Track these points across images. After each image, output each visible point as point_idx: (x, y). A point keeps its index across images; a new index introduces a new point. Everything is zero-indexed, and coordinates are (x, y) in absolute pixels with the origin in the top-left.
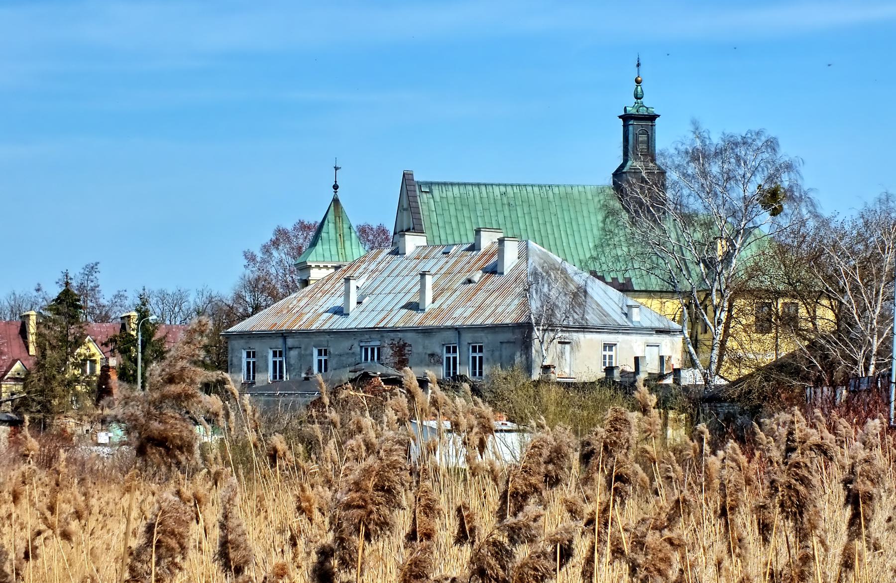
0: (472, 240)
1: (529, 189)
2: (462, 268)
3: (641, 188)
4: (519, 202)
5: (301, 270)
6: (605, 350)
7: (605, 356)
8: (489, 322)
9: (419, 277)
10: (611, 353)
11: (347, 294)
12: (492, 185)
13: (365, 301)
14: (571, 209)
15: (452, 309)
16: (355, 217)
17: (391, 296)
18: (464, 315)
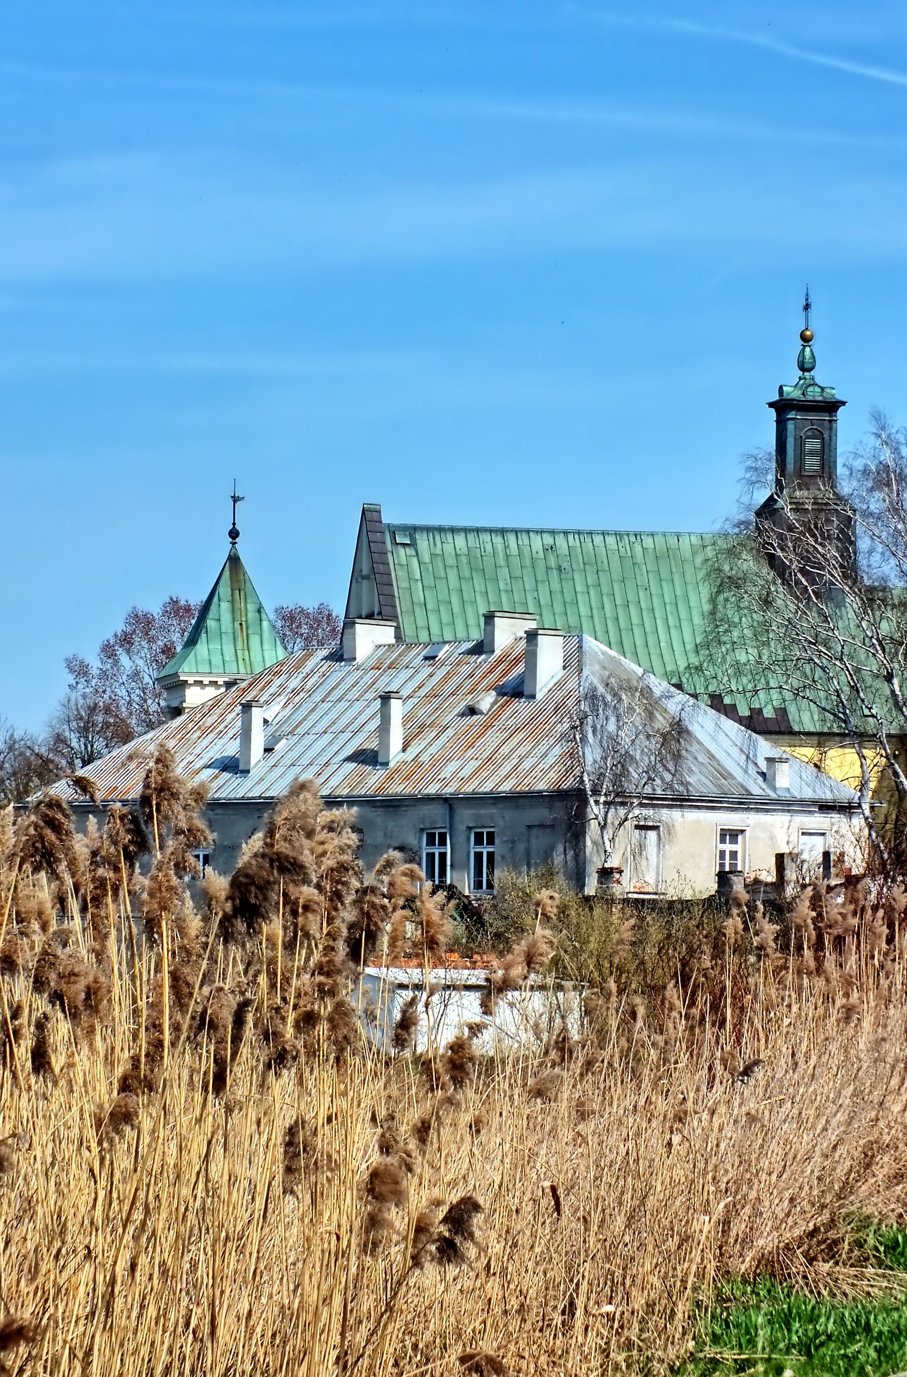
0: (476, 635)
1: (598, 539)
2: (459, 686)
3: (781, 537)
4: (578, 565)
5: (168, 688)
6: (723, 841)
7: (722, 853)
8: (506, 787)
9: (378, 704)
10: (733, 847)
11: (246, 734)
12: (528, 532)
13: (280, 747)
14: (677, 578)
15: (439, 762)
16: (276, 587)
17: (327, 738)
18: (462, 774)
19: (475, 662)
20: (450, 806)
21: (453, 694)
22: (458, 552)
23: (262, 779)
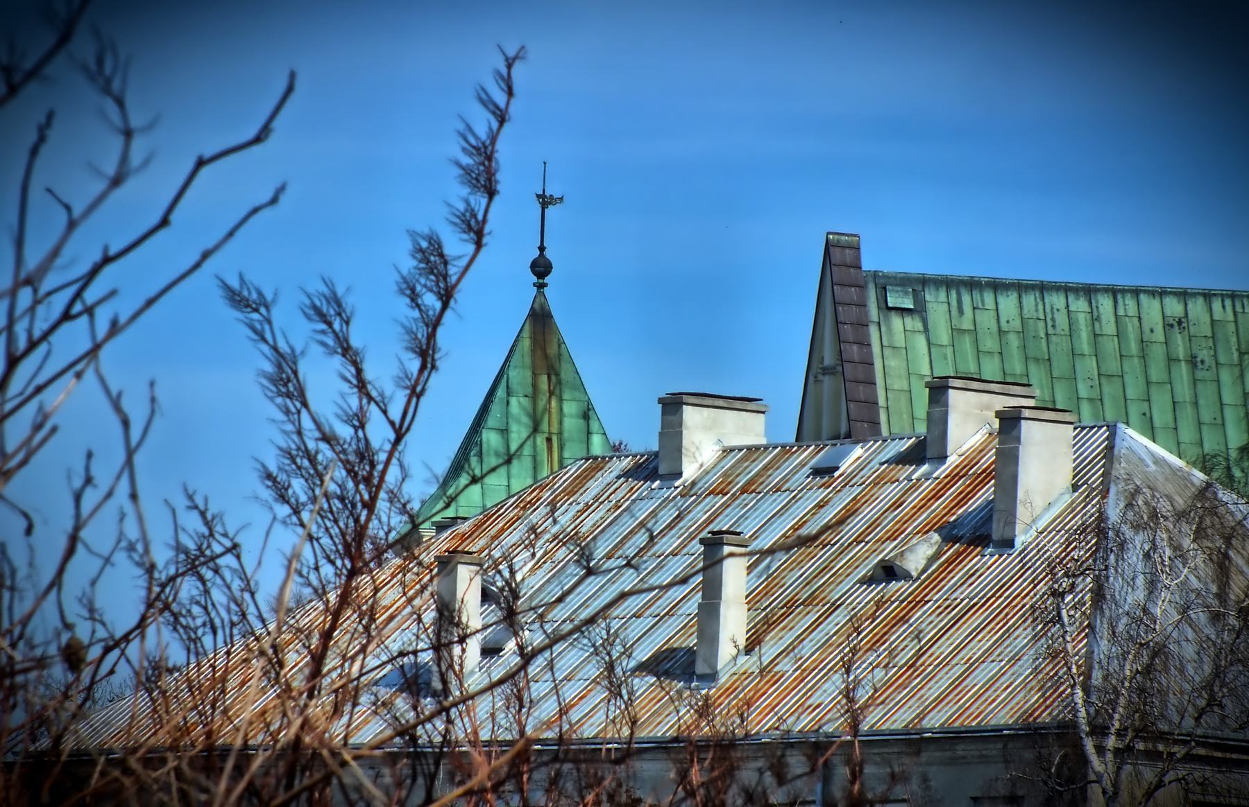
2: (873, 525)
8: (935, 721)
19: (909, 479)
21: (858, 541)
22: (1004, 326)
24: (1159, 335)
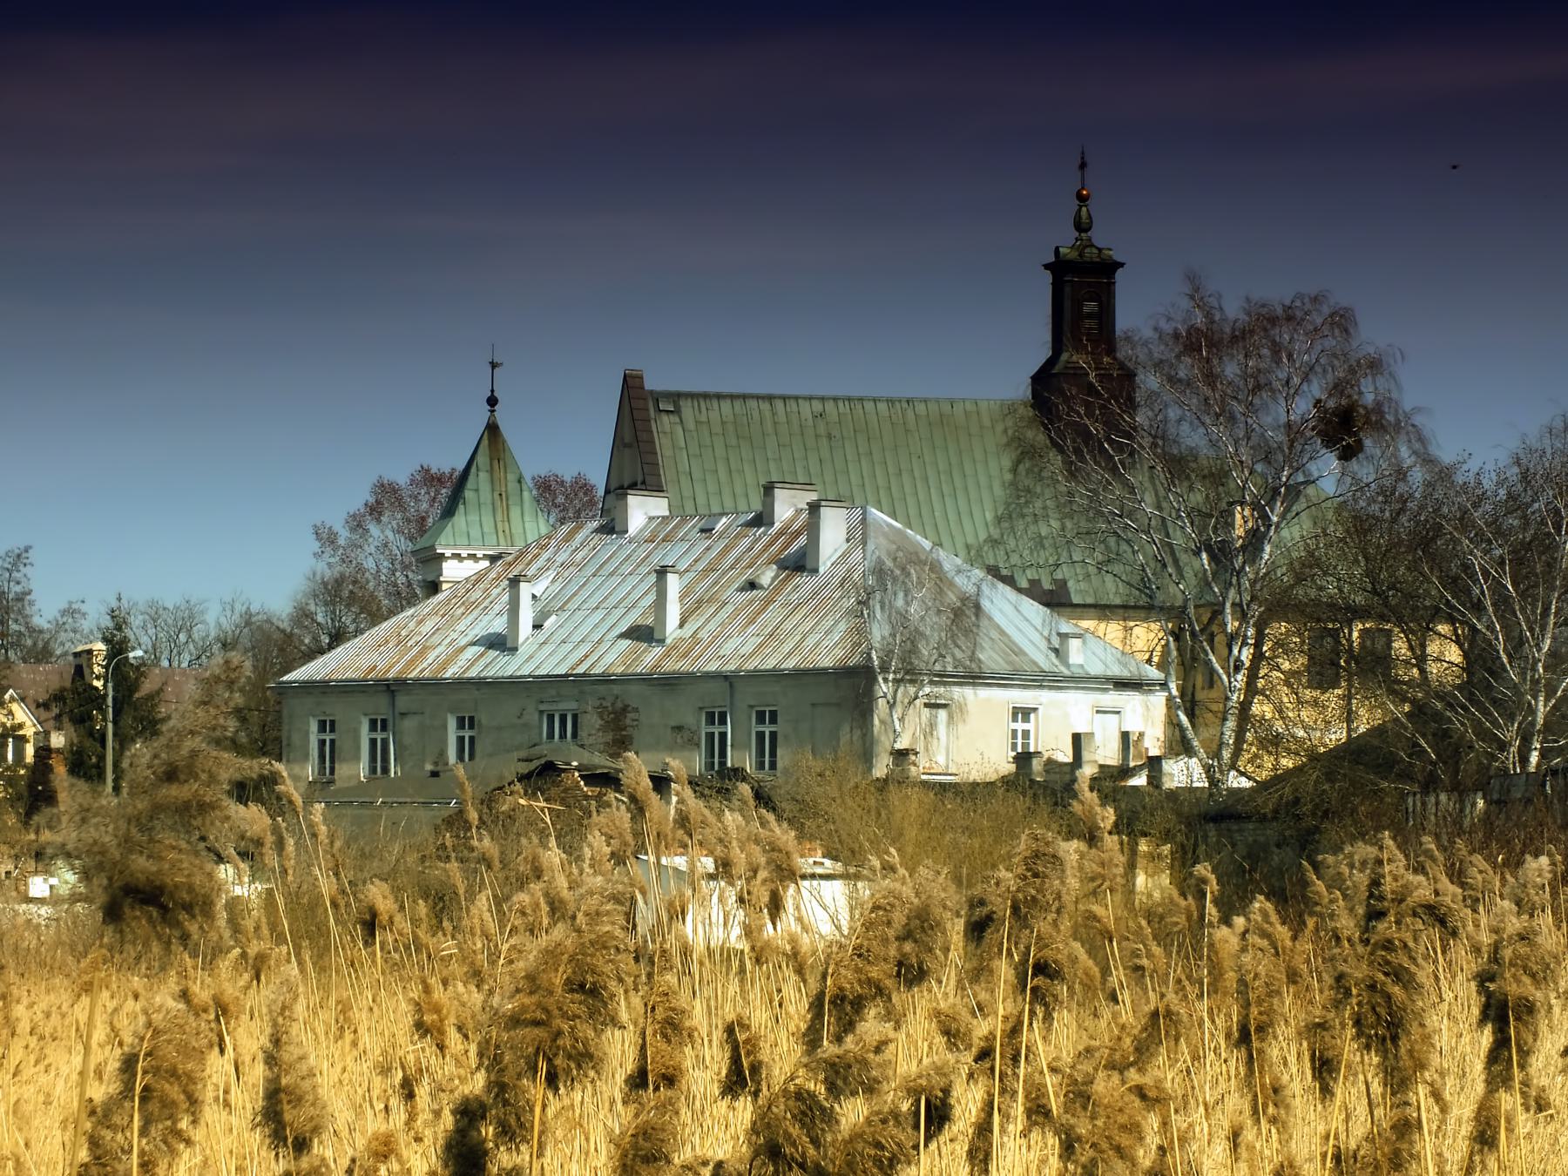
0: (757, 505)
1: (869, 406)
2: (738, 560)
3: (1088, 405)
6: (1015, 720)
7: (1014, 732)
8: (790, 664)
9: (653, 578)
10: (1026, 726)
18: (742, 651)
20: (731, 685)
21: (731, 568)
23: (531, 657)
24: (810, 422)
